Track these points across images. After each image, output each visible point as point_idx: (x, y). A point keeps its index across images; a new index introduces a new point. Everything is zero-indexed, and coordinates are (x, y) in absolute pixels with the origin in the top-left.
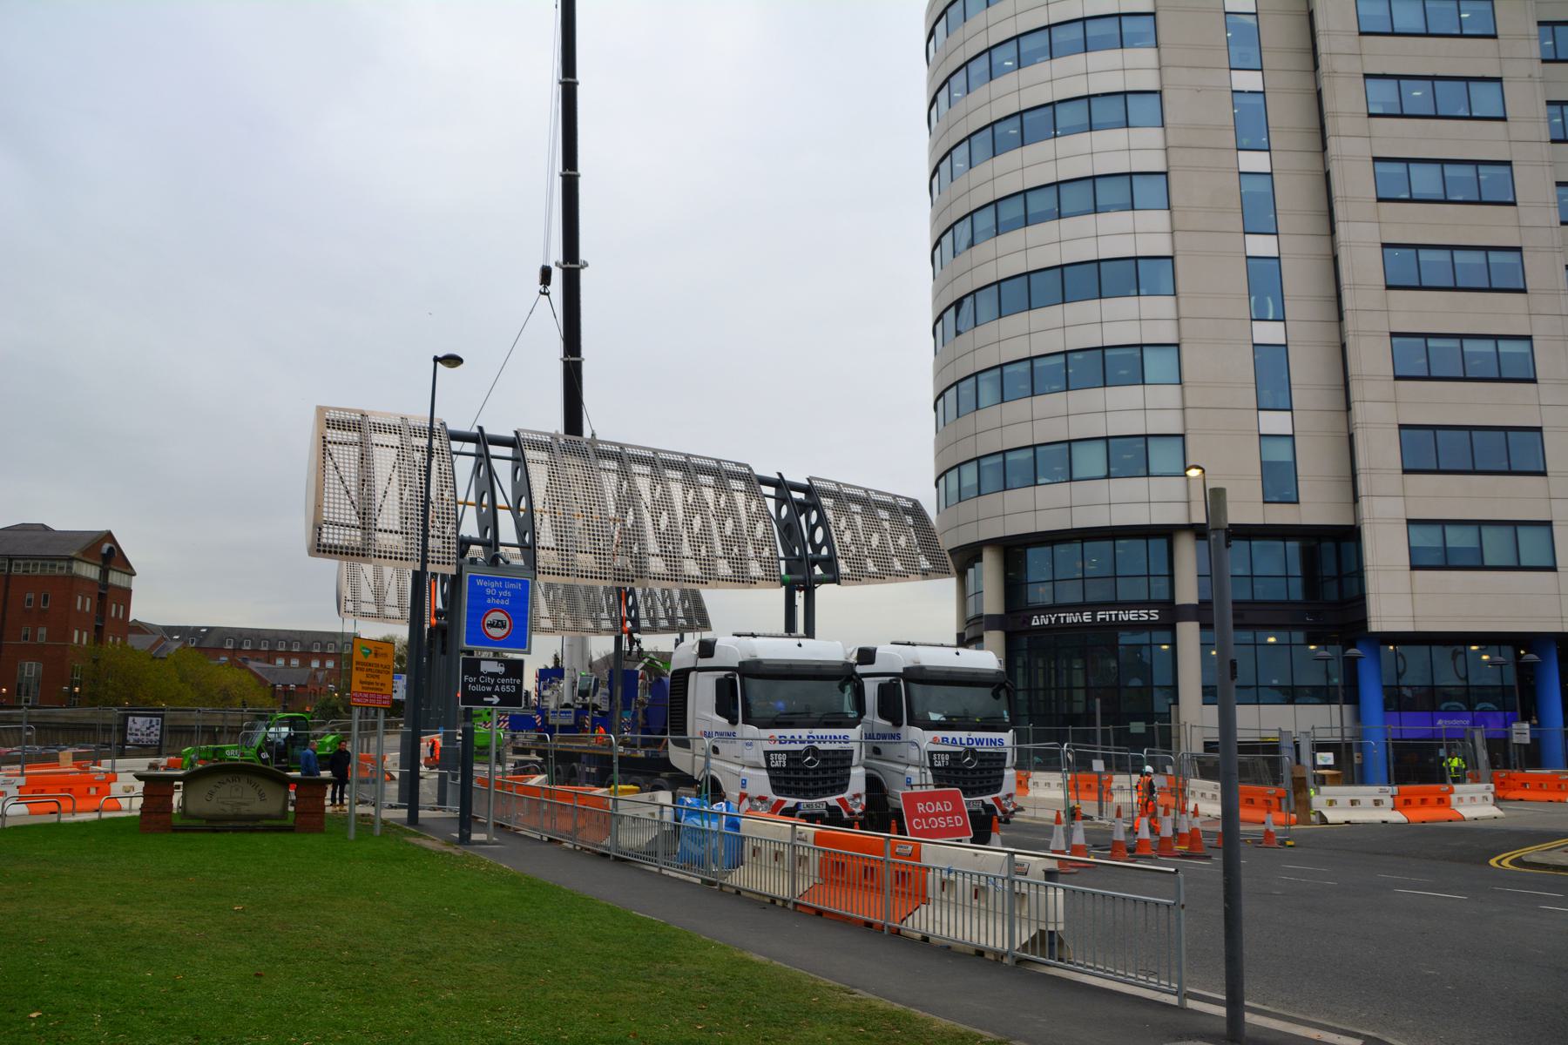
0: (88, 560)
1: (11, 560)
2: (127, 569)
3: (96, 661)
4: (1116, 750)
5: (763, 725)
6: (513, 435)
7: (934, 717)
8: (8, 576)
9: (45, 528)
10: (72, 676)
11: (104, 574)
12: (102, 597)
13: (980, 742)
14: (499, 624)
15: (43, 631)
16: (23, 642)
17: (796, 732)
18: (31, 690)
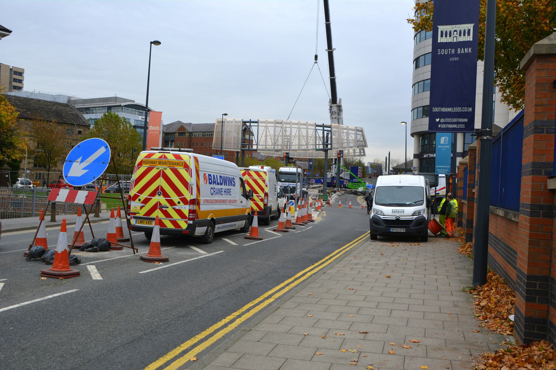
6: (257, 121)
7: (282, 180)
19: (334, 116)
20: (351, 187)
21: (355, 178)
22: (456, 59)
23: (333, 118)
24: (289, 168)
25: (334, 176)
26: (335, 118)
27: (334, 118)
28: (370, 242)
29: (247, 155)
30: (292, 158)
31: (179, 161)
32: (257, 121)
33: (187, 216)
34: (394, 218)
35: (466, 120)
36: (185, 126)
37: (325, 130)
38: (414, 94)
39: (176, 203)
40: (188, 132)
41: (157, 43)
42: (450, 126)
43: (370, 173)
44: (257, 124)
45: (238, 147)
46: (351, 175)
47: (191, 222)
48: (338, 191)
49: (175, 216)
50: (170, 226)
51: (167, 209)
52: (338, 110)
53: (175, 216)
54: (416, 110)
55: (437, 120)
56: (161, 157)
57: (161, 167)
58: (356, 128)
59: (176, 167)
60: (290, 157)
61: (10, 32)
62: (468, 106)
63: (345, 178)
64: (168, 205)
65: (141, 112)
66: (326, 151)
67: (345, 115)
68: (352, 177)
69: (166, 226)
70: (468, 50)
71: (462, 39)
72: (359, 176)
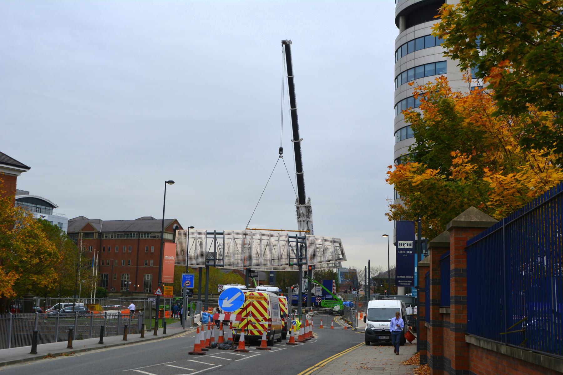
4: (93, 297)
8: (139, 240)
9: (152, 218)
14: (188, 283)
15: (152, 262)
16: (145, 266)
19: (302, 219)
21: (328, 294)
22: (406, 255)
23: (301, 221)
24: (267, 287)
25: (304, 292)
26: (304, 221)
27: (302, 221)
28: (365, 346)
30: (254, 272)
31: (261, 296)
33: (267, 328)
34: (381, 330)
35: (411, 282)
36: (92, 224)
38: (397, 142)
39: (261, 320)
40: (98, 232)
41: (171, 182)
42: (404, 284)
43: (340, 282)
44: (223, 235)
45: (201, 261)
47: (269, 331)
48: (310, 311)
49: (260, 328)
51: (256, 324)
53: (260, 328)
54: (404, 102)
55: (399, 281)
56: (250, 294)
57: (251, 300)
59: (260, 300)
60: (251, 270)
61: (29, 168)
62: (412, 276)
63: (317, 294)
64: (256, 322)
65: (39, 208)
66: (300, 266)
67: (315, 217)
68: (324, 293)
69: (254, 334)
70: (411, 252)
71: (408, 247)
72: (333, 291)
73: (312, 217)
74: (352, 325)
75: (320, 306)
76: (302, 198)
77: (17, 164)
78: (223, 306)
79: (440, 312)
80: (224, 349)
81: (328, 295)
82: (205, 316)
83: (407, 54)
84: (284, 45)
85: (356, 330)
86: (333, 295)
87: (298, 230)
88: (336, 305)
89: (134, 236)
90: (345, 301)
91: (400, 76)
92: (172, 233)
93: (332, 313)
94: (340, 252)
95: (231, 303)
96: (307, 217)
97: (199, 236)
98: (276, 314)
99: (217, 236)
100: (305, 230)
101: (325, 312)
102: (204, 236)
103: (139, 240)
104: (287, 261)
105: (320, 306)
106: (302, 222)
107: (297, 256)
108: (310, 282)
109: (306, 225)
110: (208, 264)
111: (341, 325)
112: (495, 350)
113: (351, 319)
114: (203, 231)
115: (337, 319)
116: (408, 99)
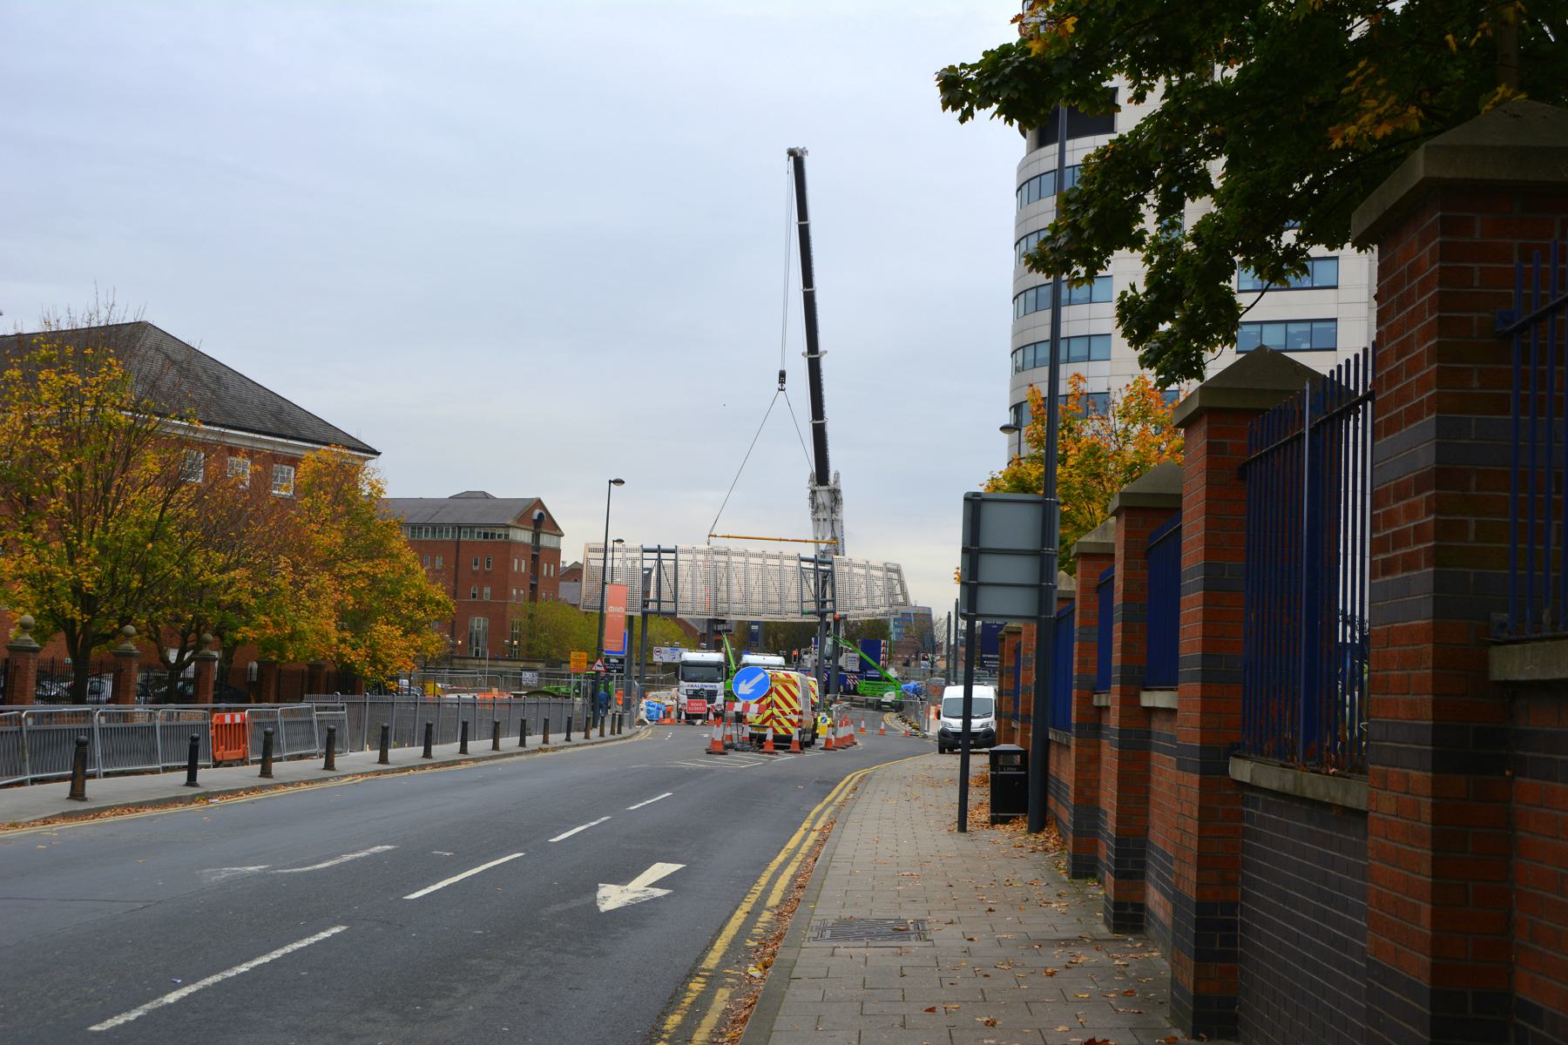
0: (521, 526)
1: (460, 528)
2: (556, 531)
3: (531, 616)
5: (686, 681)
6: (674, 548)
8: (458, 542)
9: (486, 496)
10: (513, 629)
11: (536, 537)
12: (535, 557)
13: (706, 686)
15: (487, 590)
16: (472, 600)
17: (697, 684)
18: (481, 642)
19: (821, 515)
20: (866, 692)
23: (819, 520)
24: (763, 657)
26: (825, 520)
27: (822, 520)
29: (515, 592)
32: (674, 548)
37: (821, 570)
41: (619, 482)
44: (674, 555)
46: (861, 659)
49: (787, 724)
50: (782, 732)
52: (832, 502)
53: (787, 724)
54: (1032, 294)
58: (885, 564)
61: (379, 454)
63: (849, 668)
64: (781, 715)
68: (864, 666)
72: (881, 662)
73: (842, 511)
74: (918, 729)
75: (855, 692)
76: (821, 473)
77: (360, 446)
78: (739, 692)
79: (1095, 703)
80: (743, 751)
81: (870, 670)
82: (651, 708)
83: (1040, 198)
84: (792, 158)
85: (925, 737)
86: (882, 670)
87: (812, 539)
88: (887, 691)
89: (447, 535)
90: (907, 681)
91: (1024, 240)
92: (529, 528)
93: (879, 707)
94: (898, 590)
95: (751, 688)
96: (833, 511)
97: (629, 555)
98: (807, 706)
99: (663, 556)
100: (828, 538)
101: (869, 706)
102: (638, 555)
103: (458, 542)
104: (796, 607)
105: (855, 692)
106: (822, 522)
107: (816, 596)
108: (835, 644)
109: (831, 528)
110: (645, 609)
111: (898, 728)
112: (1065, 743)
113: (917, 716)
114: (637, 545)
115: (890, 718)
116: (1039, 289)
